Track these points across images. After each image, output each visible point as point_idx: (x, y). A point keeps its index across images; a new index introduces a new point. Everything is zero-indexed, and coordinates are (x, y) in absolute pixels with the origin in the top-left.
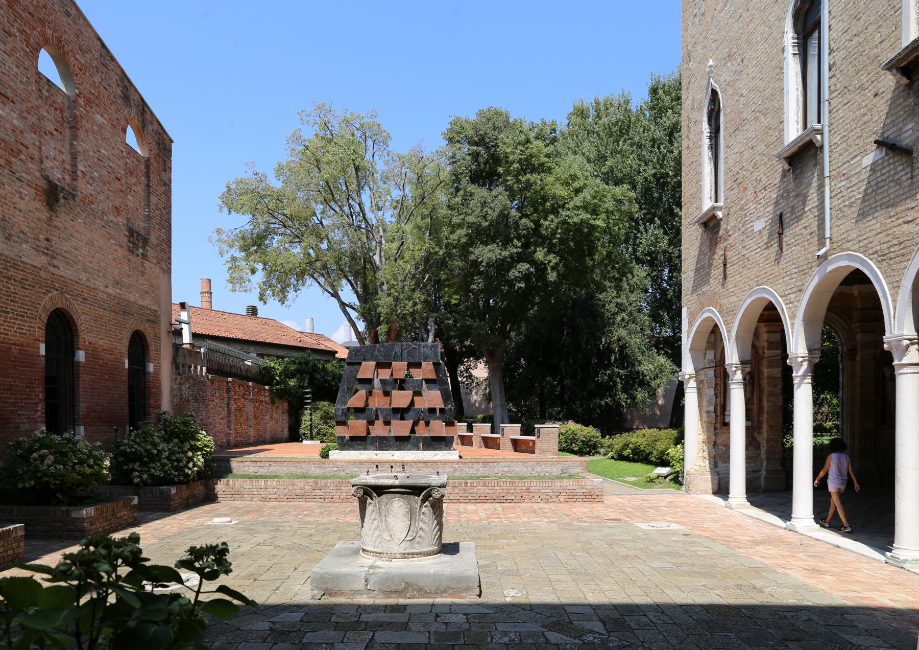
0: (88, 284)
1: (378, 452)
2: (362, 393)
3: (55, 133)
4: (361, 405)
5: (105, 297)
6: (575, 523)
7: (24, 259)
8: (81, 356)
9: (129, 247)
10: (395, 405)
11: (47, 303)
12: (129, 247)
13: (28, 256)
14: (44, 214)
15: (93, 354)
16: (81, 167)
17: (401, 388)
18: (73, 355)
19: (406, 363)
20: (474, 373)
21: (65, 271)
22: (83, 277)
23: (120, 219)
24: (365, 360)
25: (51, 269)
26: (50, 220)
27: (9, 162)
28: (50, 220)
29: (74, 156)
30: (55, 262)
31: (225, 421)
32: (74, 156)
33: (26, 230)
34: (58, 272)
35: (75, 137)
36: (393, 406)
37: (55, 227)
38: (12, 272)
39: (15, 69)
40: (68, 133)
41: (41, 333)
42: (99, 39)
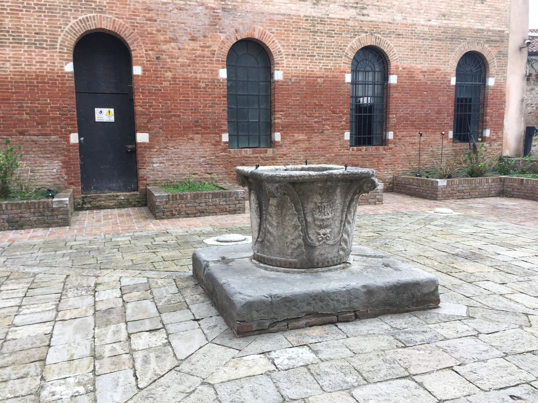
0: (405, 22)
5: (426, 29)
8: (393, 80)
15: (410, 74)
21: (374, 16)
22: (398, 17)
25: (362, 18)
30: (365, 12)
34: (369, 19)
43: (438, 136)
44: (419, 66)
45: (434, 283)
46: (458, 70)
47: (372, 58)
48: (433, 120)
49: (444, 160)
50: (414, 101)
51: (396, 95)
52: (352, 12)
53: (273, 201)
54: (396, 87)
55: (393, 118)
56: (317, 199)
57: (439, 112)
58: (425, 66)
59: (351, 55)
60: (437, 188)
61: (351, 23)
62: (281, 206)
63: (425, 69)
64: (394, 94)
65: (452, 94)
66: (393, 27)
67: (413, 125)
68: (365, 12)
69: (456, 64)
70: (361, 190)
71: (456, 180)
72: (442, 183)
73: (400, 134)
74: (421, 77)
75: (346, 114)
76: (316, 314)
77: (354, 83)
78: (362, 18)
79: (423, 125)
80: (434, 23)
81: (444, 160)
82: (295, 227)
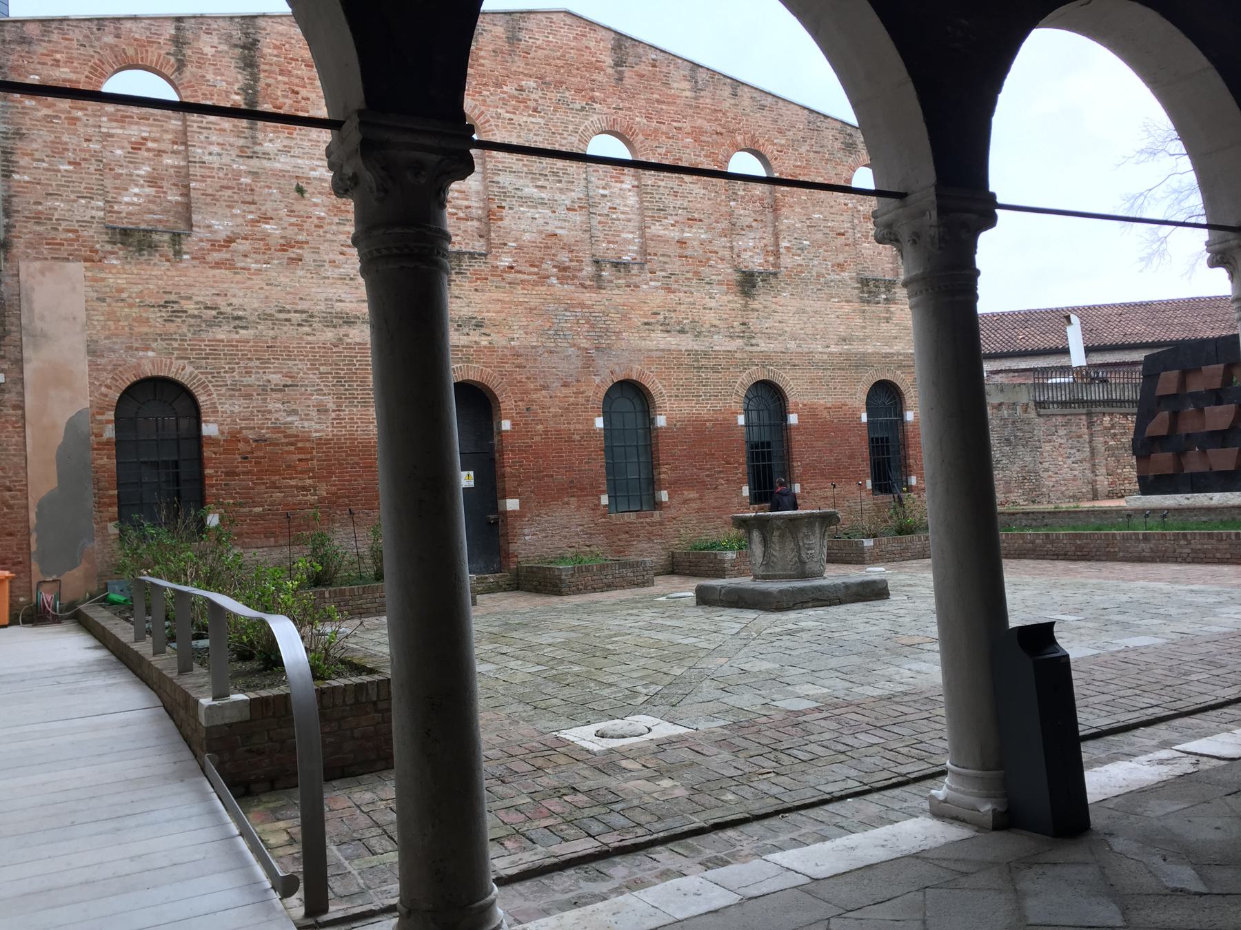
0: (799, 350)
1: (1189, 495)
2: (1164, 415)
3: (754, 224)
4: (1163, 431)
5: (825, 357)
6: (309, 482)
7: (716, 348)
8: (793, 419)
9: (861, 298)
10: (1210, 427)
11: (745, 379)
12: (861, 298)
13: (720, 345)
14: (739, 301)
15: (811, 413)
16: (784, 244)
17: (1219, 402)
18: (785, 419)
19: (1222, 366)
20: (504, 428)
21: (764, 345)
22: (792, 345)
23: (846, 275)
24: (1166, 369)
25: (750, 348)
26: (746, 305)
27: (696, 273)
28: (746, 305)
29: (776, 235)
30: (754, 341)
31: (1087, 465)
32: (776, 235)
33: (717, 323)
34: (758, 349)
35: (776, 218)
36: (1208, 429)
37: (753, 310)
38: (703, 362)
39: (703, 191)
40: (770, 217)
41: (739, 407)
42: (805, 108)
43: (854, 487)
44: (822, 402)
45: (884, 582)
46: (867, 404)
47: (768, 396)
48: (845, 467)
49: (866, 517)
50: (820, 444)
51: (799, 438)
52: (739, 342)
53: (776, 533)
54: (797, 427)
55: (798, 467)
56: (805, 530)
57: (852, 457)
58: (829, 401)
59: (742, 392)
60: (863, 548)
61: (738, 355)
62: (782, 536)
63: (829, 405)
64: (797, 437)
65: (865, 432)
66: (787, 357)
67: (823, 475)
68: (754, 341)
69: (865, 397)
70: (831, 524)
71: (884, 539)
72: (868, 543)
73: (808, 487)
74: (825, 414)
75: (741, 464)
76: (817, 600)
77: (747, 425)
78: (750, 348)
79: (834, 473)
80: (833, 349)
81: (866, 517)
82: (793, 550)
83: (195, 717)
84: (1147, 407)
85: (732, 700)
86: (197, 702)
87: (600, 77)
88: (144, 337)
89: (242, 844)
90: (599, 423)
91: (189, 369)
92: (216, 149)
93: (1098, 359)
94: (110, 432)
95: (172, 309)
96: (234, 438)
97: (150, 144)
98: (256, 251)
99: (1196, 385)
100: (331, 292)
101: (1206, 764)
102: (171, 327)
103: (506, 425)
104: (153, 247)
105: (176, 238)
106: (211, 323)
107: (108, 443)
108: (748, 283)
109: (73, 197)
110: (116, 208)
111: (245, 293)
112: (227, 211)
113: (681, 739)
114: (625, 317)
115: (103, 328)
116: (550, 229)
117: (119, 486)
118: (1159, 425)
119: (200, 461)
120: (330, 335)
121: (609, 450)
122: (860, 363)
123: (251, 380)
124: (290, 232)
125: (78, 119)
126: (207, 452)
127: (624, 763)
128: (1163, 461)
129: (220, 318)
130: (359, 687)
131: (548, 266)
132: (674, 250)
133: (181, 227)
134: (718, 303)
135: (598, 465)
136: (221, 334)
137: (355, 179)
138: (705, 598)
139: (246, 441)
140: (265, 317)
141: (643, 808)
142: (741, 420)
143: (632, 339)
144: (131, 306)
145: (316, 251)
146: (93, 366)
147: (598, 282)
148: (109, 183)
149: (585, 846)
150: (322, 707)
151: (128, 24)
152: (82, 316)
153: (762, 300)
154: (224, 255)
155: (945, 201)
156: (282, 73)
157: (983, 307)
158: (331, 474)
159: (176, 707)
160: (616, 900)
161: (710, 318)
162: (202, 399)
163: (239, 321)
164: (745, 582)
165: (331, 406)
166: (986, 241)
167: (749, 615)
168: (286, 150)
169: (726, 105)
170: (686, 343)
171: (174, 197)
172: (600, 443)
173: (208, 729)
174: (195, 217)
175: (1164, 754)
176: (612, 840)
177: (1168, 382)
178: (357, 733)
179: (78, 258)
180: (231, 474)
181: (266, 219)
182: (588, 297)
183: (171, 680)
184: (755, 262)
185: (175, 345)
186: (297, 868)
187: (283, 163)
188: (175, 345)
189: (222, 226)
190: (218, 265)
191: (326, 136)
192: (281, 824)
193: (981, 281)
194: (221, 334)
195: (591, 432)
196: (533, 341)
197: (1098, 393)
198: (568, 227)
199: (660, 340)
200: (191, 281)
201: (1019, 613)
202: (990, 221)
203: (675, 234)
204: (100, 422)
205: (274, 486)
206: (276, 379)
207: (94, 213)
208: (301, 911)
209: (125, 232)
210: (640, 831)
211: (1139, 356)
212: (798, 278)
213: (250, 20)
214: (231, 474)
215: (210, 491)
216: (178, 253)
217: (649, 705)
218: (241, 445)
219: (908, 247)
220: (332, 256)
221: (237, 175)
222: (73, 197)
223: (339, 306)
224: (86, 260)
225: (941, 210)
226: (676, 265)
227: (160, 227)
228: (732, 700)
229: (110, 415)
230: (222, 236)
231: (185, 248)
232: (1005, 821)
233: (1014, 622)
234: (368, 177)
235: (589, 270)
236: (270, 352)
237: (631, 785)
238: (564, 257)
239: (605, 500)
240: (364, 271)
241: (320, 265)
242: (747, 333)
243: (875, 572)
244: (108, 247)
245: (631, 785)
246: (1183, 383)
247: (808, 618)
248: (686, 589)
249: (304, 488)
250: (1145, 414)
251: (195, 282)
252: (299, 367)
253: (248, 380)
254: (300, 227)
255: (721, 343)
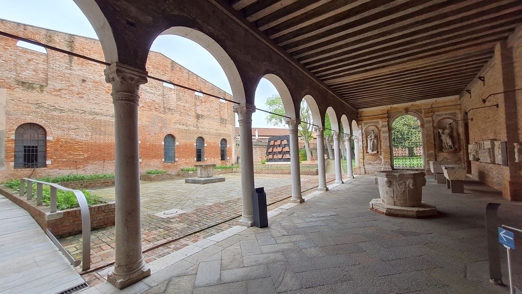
15: (209, 144)
21: (201, 129)
41: (195, 142)
47: (201, 140)
83: (44, 218)
84: (269, 147)
85: (195, 204)
86: (44, 214)
87: (168, 69)
88: (29, 112)
89: (60, 253)
90: (163, 143)
91: (44, 122)
92: (57, 66)
93: (260, 137)
94: (13, 137)
95: (39, 105)
96: (58, 140)
97: (34, 61)
98: (69, 93)
99: (276, 143)
100: (92, 106)
101: (283, 210)
102: (38, 110)
103: (139, 142)
104: (33, 88)
105: (42, 86)
106: (52, 110)
107: (12, 140)
108: (198, 117)
109: (4, 70)
110: (20, 75)
111: (66, 103)
112: (60, 82)
113: (185, 214)
114: (170, 121)
115: (13, 108)
116: (153, 99)
117: (15, 152)
118: (270, 150)
119: (45, 146)
120: (91, 117)
121: (165, 149)
122: (220, 135)
123: (65, 126)
124: (80, 90)
125: (8, 49)
126: (48, 144)
127: (171, 220)
128: (271, 156)
129: (56, 109)
130: (99, 207)
131: (152, 107)
132: (182, 108)
133: (44, 84)
134: (192, 120)
135: (163, 152)
136: (55, 113)
137: (113, 79)
138: (187, 182)
139: (62, 142)
140: (70, 110)
141: (177, 230)
142: (195, 144)
143: (172, 126)
144: (24, 103)
145: (88, 96)
146: (8, 119)
147: (164, 112)
148: (18, 69)
149: (164, 241)
150: (91, 212)
151: (29, 27)
152: (5, 104)
153: (201, 120)
154: (58, 93)
155: (248, 107)
156: (81, 51)
157: (252, 127)
158: (88, 151)
159: (37, 216)
160: (173, 254)
161: (190, 123)
162: (47, 130)
163: (62, 111)
164: (197, 178)
165: (90, 134)
166: (253, 114)
167: (197, 185)
168: (81, 70)
169: (195, 80)
170: (184, 127)
171: (42, 76)
172: (163, 147)
173: (48, 222)
174: (49, 82)
175: (276, 209)
176: (170, 239)
177: (272, 143)
178: (98, 219)
179: (4, 87)
180: (56, 150)
181: (73, 86)
182: (162, 115)
183: (34, 208)
184: (200, 113)
185: (39, 115)
186: (80, 257)
187: (79, 73)
188: (39, 115)
189: (58, 86)
190: (56, 95)
191: (105, 67)
192: (73, 245)
193: (252, 122)
194: (55, 113)
195: (160, 145)
196: (147, 123)
197: (260, 144)
198: (159, 99)
199: (178, 126)
200: (46, 99)
201: (257, 186)
202: (255, 111)
203: (183, 104)
204: (9, 134)
205: (70, 154)
206: (73, 127)
207: (12, 76)
208: (81, 270)
209: (23, 83)
210: (177, 236)
211: (268, 138)
212: (208, 117)
213: (71, 36)
214: (56, 150)
215: (48, 155)
216: (42, 91)
217: (175, 206)
218: (60, 143)
219: (240, 114)
220: (93, 98)
221: (64, 74)
222: (4, 70)
223: (94, 110)
224: (7, 88)
225: (246, 108)
226: (183, 111)
227: (36, 83)
228: (195, 204)
229: (14, 132)
230: (58, 88)
231: (45, 90)
232: (252, 225)
233: (256, 187)
234: (118, 79)
235: (162, 109)
236: (71, 120)
237: (173, 226)
238: (156, 106)
239: (163, 160)
240: (114, 103)
241: (89, 99)
242: (197, 127)
243: (221, 176)
244: (17, 86)
245: (173, 226)
246: (281, 142)
247: (210, 185)
248: (183, 181)
249: (80, 155)
250: (268, 149)
251: (47, 99)
252: (81, 124)
253: (63, 126)
254: (84, 89)
255: (192, 128)
